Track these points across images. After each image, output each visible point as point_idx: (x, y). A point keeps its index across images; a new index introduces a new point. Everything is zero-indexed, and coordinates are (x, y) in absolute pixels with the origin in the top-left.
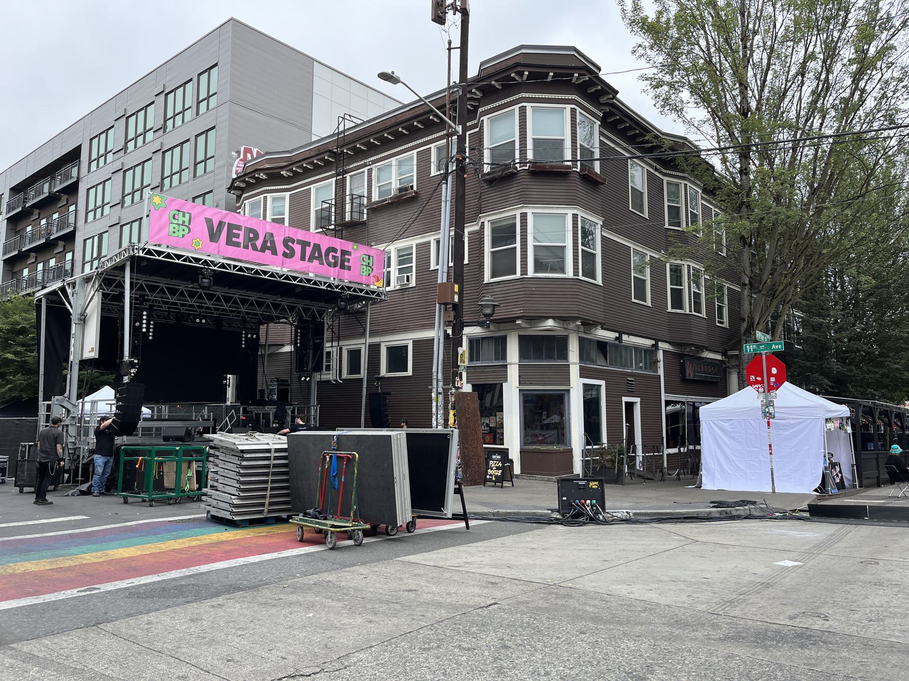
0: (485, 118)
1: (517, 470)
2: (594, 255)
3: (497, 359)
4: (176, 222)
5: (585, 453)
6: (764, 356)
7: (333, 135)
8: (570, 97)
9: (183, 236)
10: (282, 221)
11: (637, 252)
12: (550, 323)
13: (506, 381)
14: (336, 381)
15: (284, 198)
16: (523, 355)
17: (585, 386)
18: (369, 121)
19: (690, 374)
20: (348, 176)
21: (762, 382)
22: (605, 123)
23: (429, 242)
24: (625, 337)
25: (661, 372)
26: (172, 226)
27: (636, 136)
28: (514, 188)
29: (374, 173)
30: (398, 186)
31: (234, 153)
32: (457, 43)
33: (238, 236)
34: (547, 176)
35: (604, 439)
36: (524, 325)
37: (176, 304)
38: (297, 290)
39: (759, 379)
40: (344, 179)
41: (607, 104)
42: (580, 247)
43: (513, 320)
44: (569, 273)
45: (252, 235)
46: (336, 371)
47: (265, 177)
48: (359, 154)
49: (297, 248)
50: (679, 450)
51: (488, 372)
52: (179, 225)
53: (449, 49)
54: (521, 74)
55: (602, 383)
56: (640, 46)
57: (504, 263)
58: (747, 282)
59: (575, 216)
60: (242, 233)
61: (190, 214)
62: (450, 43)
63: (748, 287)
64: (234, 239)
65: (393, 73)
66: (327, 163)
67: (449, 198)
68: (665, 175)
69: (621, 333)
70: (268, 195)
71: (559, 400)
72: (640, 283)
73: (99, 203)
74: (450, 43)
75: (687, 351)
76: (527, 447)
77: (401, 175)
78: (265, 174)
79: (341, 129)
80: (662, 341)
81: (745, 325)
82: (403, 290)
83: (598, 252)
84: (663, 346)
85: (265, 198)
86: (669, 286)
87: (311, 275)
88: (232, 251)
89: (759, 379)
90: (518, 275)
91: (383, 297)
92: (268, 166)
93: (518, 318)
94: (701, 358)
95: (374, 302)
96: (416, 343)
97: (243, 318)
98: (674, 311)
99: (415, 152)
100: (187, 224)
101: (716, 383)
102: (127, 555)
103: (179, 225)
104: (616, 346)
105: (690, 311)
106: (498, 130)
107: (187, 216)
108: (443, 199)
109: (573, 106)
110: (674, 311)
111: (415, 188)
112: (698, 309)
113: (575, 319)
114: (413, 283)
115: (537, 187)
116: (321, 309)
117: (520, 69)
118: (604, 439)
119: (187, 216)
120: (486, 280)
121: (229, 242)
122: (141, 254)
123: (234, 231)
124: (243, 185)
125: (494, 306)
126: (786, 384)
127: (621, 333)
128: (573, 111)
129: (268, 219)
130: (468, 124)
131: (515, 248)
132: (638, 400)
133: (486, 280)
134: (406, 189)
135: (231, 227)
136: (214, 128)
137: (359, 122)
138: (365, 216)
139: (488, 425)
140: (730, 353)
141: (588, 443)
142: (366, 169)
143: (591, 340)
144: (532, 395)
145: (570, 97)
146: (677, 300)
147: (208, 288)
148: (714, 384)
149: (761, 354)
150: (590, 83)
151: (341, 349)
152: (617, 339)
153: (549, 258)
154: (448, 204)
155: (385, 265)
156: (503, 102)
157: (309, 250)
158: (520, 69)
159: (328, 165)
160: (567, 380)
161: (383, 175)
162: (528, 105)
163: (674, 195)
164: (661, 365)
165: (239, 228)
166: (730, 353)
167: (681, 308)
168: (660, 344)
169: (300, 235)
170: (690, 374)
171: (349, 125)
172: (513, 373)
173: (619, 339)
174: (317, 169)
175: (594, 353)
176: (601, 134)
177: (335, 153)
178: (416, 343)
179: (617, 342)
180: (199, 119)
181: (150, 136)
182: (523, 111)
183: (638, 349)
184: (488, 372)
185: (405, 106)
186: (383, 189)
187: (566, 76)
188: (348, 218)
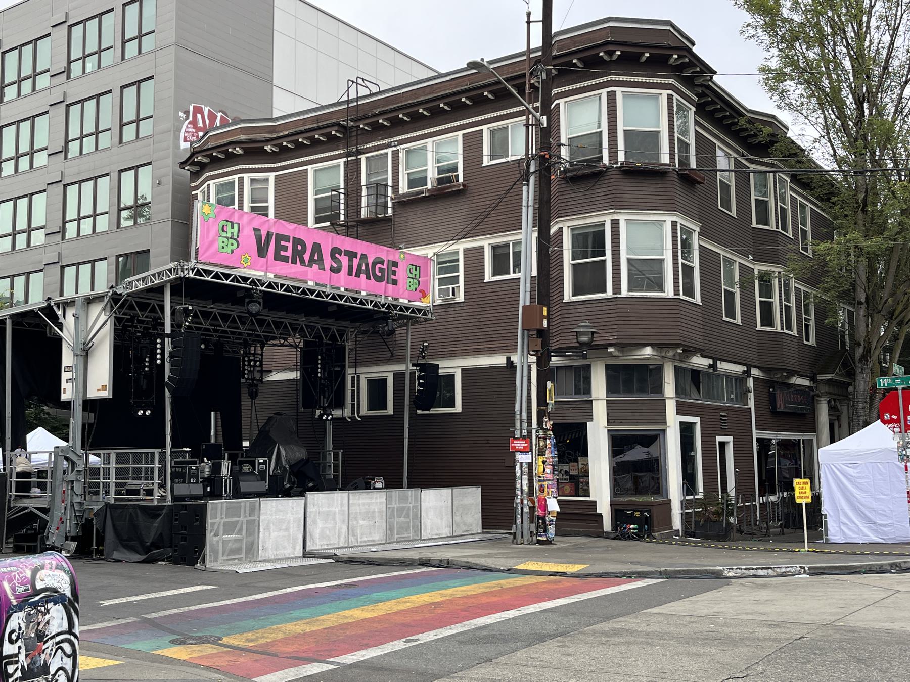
0: (561, 101)
1: (607, 525)
2: (692, 268)
3: (577, 392)
4: (224, 234)
5: (685, 504)
6: (900, 392)
7: (339, 103)
8: (667, 81)
9: (232, 251)
10: (264, 211)
11: (726, 260)
12: (648, 351)
13: (592, 420)
14: (353, 419)
16: (611, 388)
17: (681, 423)
18: (393, 90)
19: (781, 406)
20: (363, 157)
21: (898, 421)
22: (701, 110)
25: (751, 404)
26: (221, 239)
27: (716, 110)
28: (601, 190)
29: (402, 155)
30: (436, 176)
31: (181, 114)
32: (537, 14)
33: (285, 249)
34: (643, 179)
35: (701, 487)
36: (617, 353)
37: (208, 330)
38: (330, 309)
39: (894, 417)
40: (358, 161)
41: (702, 86)
42: (680, 261)
43: (605, 346)
44: (669, 292)
45: (299, 247)
46: (357, 404)
47: (241, 152)
48: (377, 130)
49: (344, 260)
50: (767, 499)
51: (568, 409)
52: (228, 238)
53: (529, 22)
54: (610, 53)
56: (749, 25)
57: (587, 278)
58: (863, 300)
59: (674, 224)
60: (290, 245)
61: (239, 224)
62: (529, 15)
63: (864, 306)
64: (282, 253)
65: (482, 60)
66: (332, 139)
67: (531, 203)
68: (752, 161)
69: (715, 360)
72: (730, 295)
74: (529, 15)
75: (777, 377)
76: (622, 499)
77: (439, 162)
78: (241, 148)
79: (353, 95)
80: (722, 360)
81: (860, 351)
82: (447, 306)
83: (696, 264)
84: (755, 372)
85: (241, 180)
86: (758, 299)
87: (311, 284)
88: (294, 270)
89: (894, 417)
90: (610, 293)
91: (430, 316)
92: (243, 137)
93: (611, 345)
94: (789, 384)
95: (416, 321)
96: (465, 371)
97: (245, 340)
98: (763, 329)
99: (460, 133)
100: (235, 237)
101: (804, 415)
103: (228, 238)
104: (709, 374)
105: (782, 329)
106: (580, 116)
107: (236, 226)
108: (524, 203)
109: (670, 92)
110: (763, 329)
111: (461, 180)
112: (789, 327)
113: (678, 345)
114: (461, 298)
115: (630, 188)
116: (333, 330)
117: (611, 48)
118: (701, 487)
119: (236, 226)
120: (487, 280)
121: (278, 257)
122: (191, 275)
123: (283, 243)
124: (205, 160)
125: (593, 333)
127: (715, 360)
128: (670, 97)
129: (246, 208)
131: (605, 261)
132: (730, 439)
133: (487, 280)
134: (449, 180)
135: (279, 237)
136: (151, 78)
137: (375, 90)
138: (390, 211)
139: (567, 473)
140: (820, 377)
142: (389, 151)
143: (684, 369)
145: (667, 81)
146: (768, 319)
147: (258, 313)
148: (802, 416)
149: (896, 389)
150: (690, 65)
151: (358, 377)
152: (710, 366)
153: (646, 273)
154: (531, 209)
155: (425, 273)
156: (586, 84)
157: (356, 262)
158: (611, 48)
159: (331, 142)
161: (414, 159)
162: (619, 90)
163: (763, 187)
164: (751, 395)
165: (287, 239)
166: (820, 377)
167: (771, 325)
169: (289, 229)
170: (781, 406)
171: (363, 92)
172: (600, 409)
173: (713, 366)
174: (315, 146)
175: (689, 386)
176: (697, 123)
177: (343, 126)
178: (465, 371)
179: (711, 371)
180: (125, 65)
181: (43, 81)
182: (612, 97)
183: (729, 376)
184: (568, 409)
185: (441, 76)
186: (412, 177)
187: (656, 54)
188: (364, 213)
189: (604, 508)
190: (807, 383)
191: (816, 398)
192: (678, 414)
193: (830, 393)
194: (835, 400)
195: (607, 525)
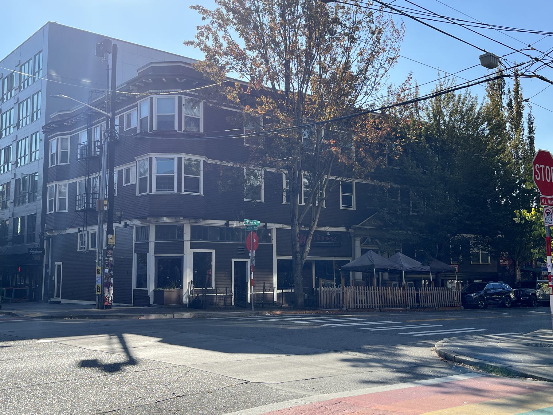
15: (67, 138)
20: (93, 127)
23: (122, 170)
55: (213, 251)
70: (59, 137)
71: (179, 263)
73: (24, 116)
85: (58, 139)
102: (360, 394)
130: (116, 112)
142: (100, 124)
152: (226, 224)
160: (181, 249)
173: (227, 224)
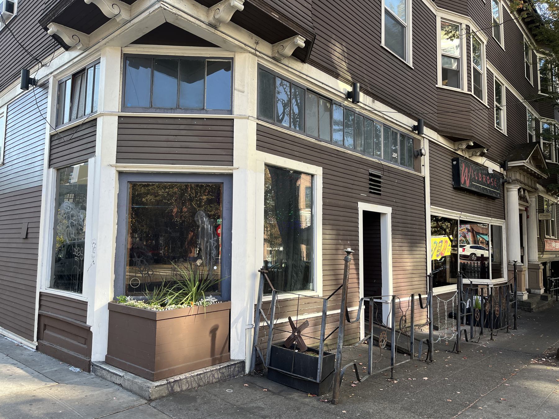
1: (99, 350)
19: (465, 181)
24: (363, 97)
25: (426, 172)
126: (231, 358)
132: (387, 210)
140: (511, 164)
141: (266, 290)
144: (172, 185)
160: (226, 153)
168: (426, 131)
189: (98, 321)
190: (493, 167)
191: (506, 186)
192: (85, 304)
193: (521, 182)
194: (524, 190)
195: (99, 350)
